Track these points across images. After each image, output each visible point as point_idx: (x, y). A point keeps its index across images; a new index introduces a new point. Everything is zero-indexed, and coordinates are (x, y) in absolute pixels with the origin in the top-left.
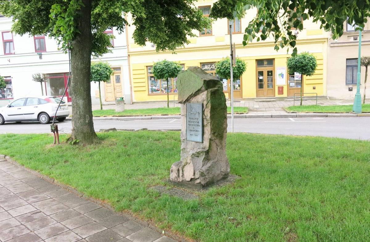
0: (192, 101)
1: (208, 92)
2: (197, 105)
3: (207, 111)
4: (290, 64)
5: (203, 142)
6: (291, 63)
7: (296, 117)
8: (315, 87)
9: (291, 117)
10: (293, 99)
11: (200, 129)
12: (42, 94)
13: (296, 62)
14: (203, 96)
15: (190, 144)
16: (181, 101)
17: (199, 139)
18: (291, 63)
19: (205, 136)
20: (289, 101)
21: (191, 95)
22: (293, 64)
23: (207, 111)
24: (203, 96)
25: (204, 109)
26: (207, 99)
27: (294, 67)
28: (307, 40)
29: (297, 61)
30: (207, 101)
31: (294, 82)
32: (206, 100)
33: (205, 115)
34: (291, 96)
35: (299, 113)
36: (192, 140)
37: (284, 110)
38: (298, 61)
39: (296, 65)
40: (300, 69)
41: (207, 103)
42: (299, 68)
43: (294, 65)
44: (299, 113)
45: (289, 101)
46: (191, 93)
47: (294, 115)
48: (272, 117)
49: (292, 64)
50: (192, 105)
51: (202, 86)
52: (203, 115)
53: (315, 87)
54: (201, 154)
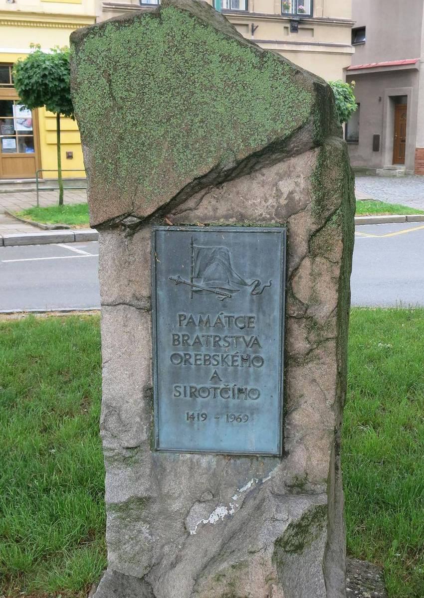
0: (199, 212)
1: (322, 158)
2: (247, 239)
3: (314, 276)
4: (26, 81)
5: (284, 454)
6: (29, 78)
7: (75, 241)
8: (71, 153)
9: (60, 240)
10: (34, 187)
11: (268, 380)
12: (80, 5)
13: (44, 76)
14: (286, 186)
15: (185, 469)
16: (113, 211)
17: (260, 435)
18: (29, 78)
19: (297, 417)
20: (6, 192)
21: (203, 177)
22: (37, 82)
23: (314, 276)
24: (286, 186)
25: (293, 264)
26: (319, 201)
27: (39, 91)
28: (44, 15)
29: (47, 73)
30: (319, 216)
31: (15, 138)
32: (311, 205)
33: (299, 296)
34: (10, 176)
35: (75, 227)
36: (207, 443)
37: (20, 220)
38: (50, 74)
39: (46, 85)
40: (56, 99)
41: (314, 227)
42: (53, 94)
43: (40, 85)
44: (75, 227)
45: (6, 192)
46: (211, 163)
47: (68, 236)
48: (3, 245)
49: (33, 81)
50: (202, 237)
51: (282, 129)
52: (290, 300)
53: (71, 153)
54: (313, 529)
